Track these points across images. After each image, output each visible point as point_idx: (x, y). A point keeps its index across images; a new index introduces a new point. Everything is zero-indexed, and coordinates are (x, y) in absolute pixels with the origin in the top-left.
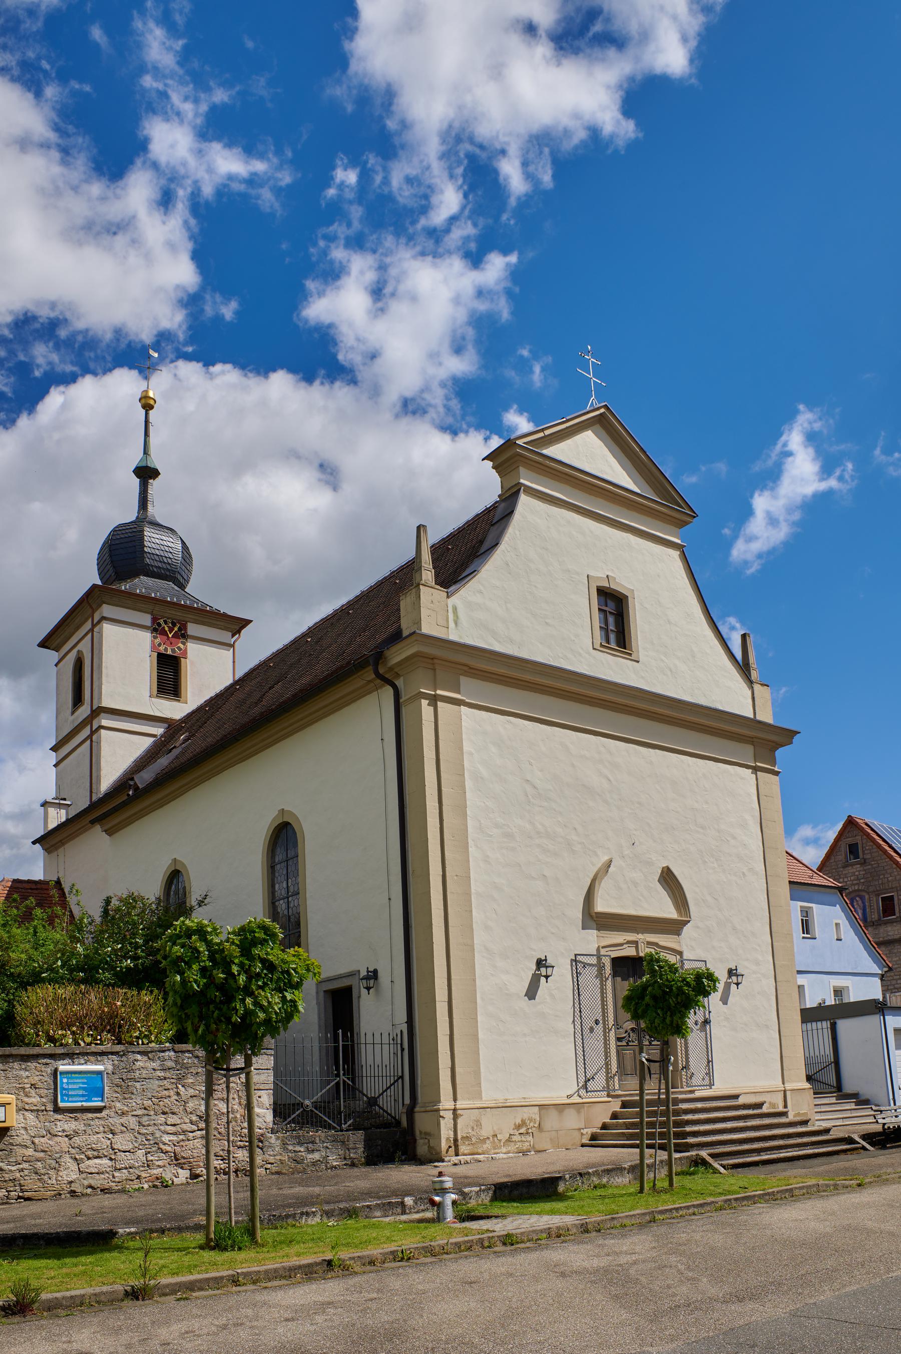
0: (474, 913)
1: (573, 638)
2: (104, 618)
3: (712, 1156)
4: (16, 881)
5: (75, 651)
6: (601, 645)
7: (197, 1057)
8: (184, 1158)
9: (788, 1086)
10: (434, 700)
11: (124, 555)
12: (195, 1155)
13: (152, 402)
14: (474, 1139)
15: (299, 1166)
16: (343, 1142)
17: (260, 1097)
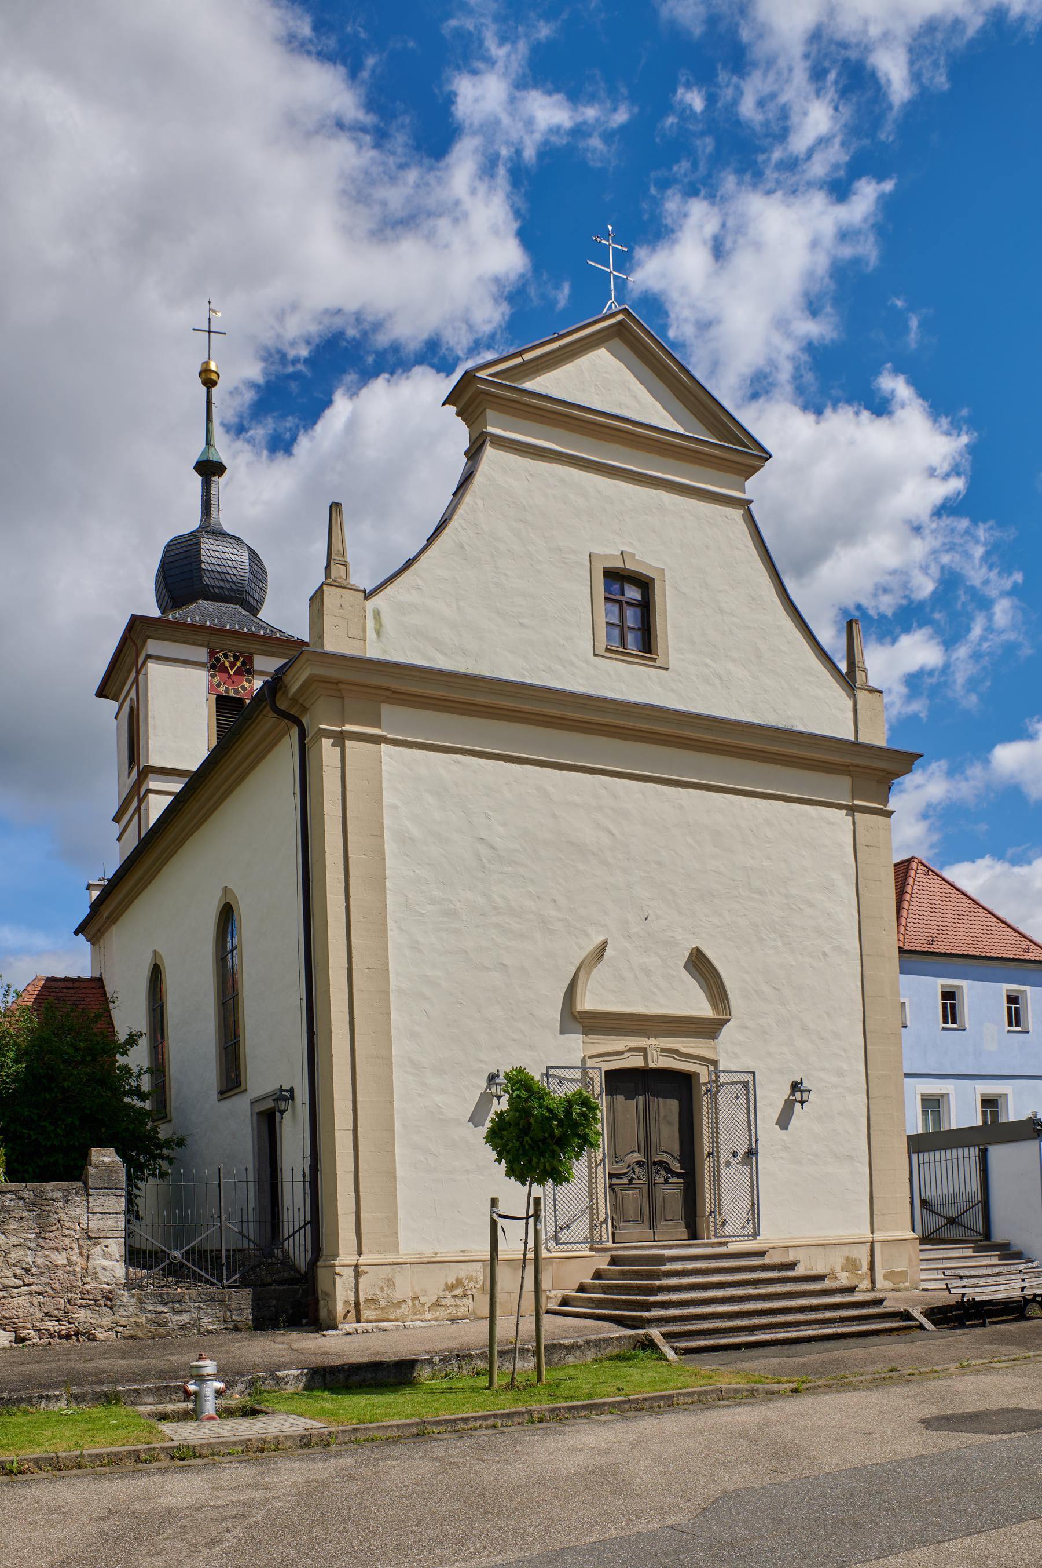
0: (394, 1016)
1: (562, 642)
2: (149, 657)
3: (665, 1336)
4: (50, 980)
5: (128, 699)
6: (607, 650)
7: (22, 1198)
8: (7, 1318)
9: (879, 1236)
10: (340, 739)
11: (182, 572)
12: (21, 1314)
13: (214, 377)
14: (383, 1303)
15: (161, 1329)
16: (223, 1302)
17: (106, 1247)
